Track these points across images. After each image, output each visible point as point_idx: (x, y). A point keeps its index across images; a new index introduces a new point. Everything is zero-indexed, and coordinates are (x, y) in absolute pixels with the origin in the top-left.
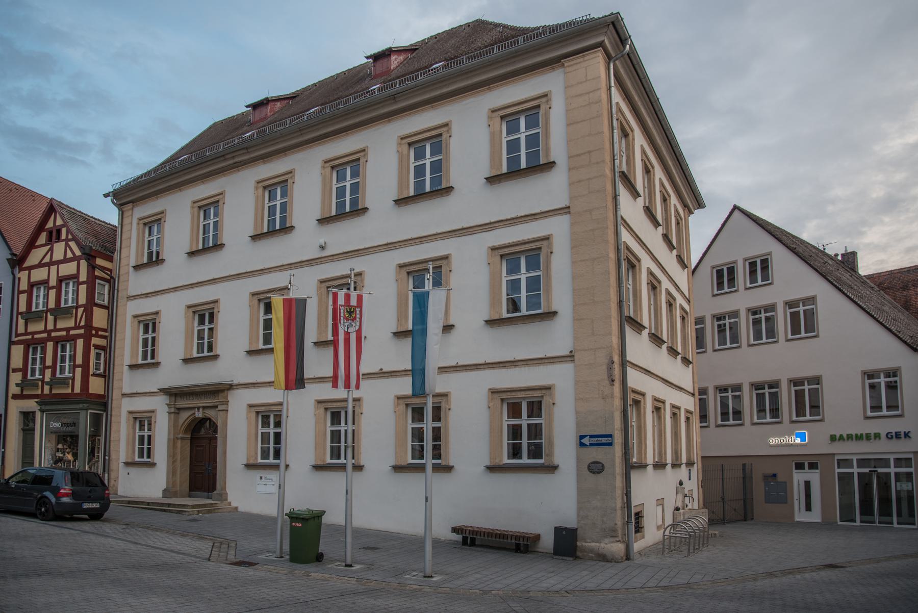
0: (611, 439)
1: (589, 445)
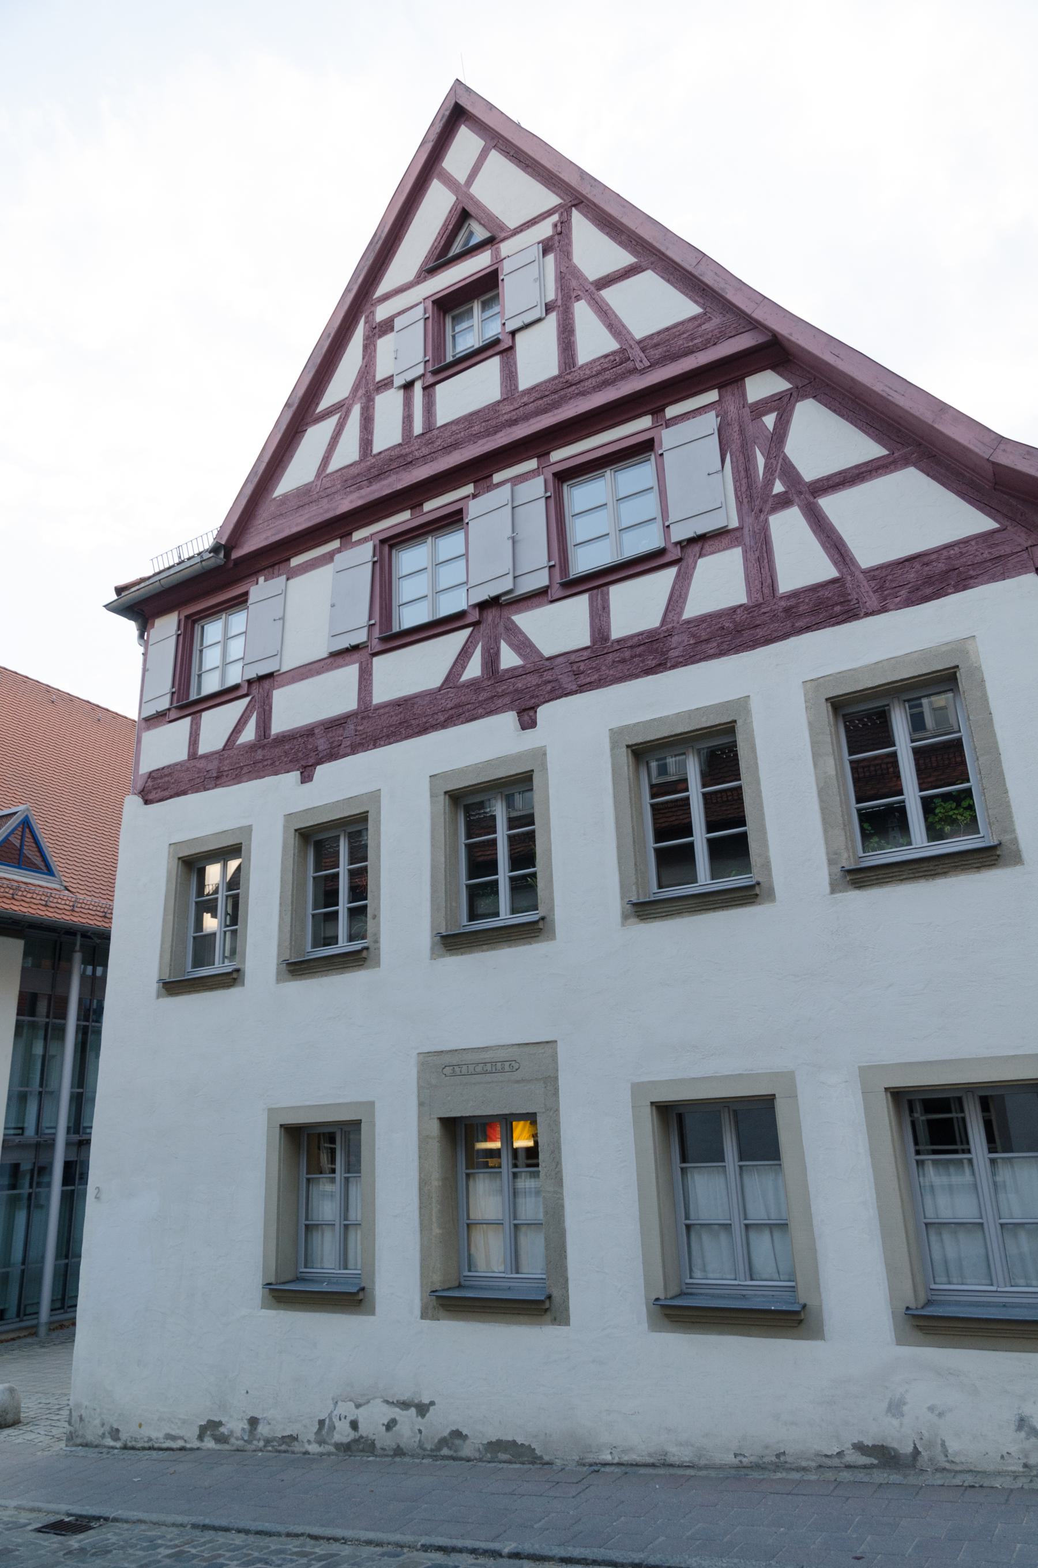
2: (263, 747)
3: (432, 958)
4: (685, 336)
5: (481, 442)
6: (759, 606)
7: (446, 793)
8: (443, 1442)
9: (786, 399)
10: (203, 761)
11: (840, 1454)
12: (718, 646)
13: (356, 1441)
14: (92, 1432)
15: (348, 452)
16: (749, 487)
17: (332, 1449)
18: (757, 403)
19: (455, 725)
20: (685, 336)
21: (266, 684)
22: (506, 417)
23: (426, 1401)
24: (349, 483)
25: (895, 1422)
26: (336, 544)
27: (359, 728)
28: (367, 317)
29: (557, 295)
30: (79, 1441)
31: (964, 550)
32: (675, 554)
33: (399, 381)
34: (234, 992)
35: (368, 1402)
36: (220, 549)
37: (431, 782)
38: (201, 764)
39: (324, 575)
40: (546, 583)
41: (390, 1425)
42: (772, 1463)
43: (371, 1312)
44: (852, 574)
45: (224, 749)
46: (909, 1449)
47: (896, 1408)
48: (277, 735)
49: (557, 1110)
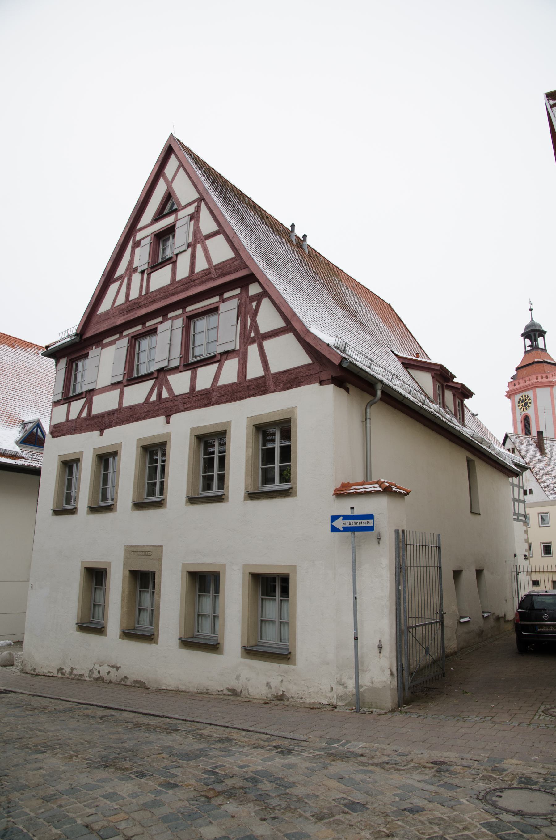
0: (371, 521)
1: (342, 529)
2: (89, 420)
3: (132, 511)
4: (228, 266)
5: (163, 301)
6: (240, 384)
7: (141, 446)
8: (122, 679)
9: (260, 296)
10: (70, 423)
11: (222, 691)
12: (226, 398)
13: (99, 678)
14: (28, 669)
15: (121, 300)
16: (244, 332)
17: (92, 679)
18: (252, 296)
19: (147, 419)
20: (228, 266)
21: (92, 393)
22: (171, 292)
23: (118, 666)
24: (121, 312)
25: (237, 682)
26: (117, 336)
27: (118, 416)
28: (134, 238)
29: (192, 240)
30: (24, 671)
31: (301, 370)
32: (218, 358)
33: (139, 270)
34: (74, 516)
35: (103, 665)
36: (80, 334)
37: (137, 441)
38: (70, 424)
39: (112, 348)
40: (178, 364)
41: (109, 672)
42: (205, 692)
43: (106, 635)
44: (268, 375)
45: (77, 419)
46: (239, 691)
47: (238, 677)
48: (93, 415)
49: (161, 571)
